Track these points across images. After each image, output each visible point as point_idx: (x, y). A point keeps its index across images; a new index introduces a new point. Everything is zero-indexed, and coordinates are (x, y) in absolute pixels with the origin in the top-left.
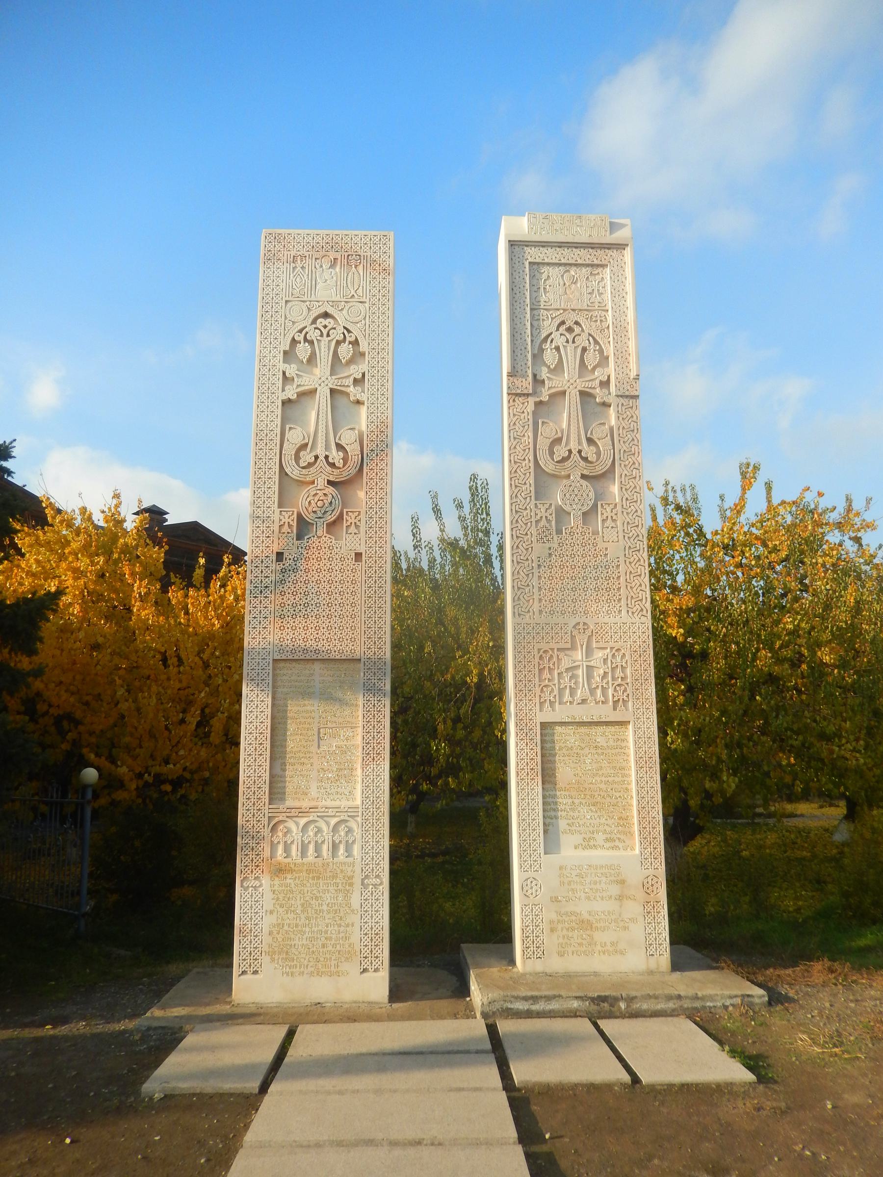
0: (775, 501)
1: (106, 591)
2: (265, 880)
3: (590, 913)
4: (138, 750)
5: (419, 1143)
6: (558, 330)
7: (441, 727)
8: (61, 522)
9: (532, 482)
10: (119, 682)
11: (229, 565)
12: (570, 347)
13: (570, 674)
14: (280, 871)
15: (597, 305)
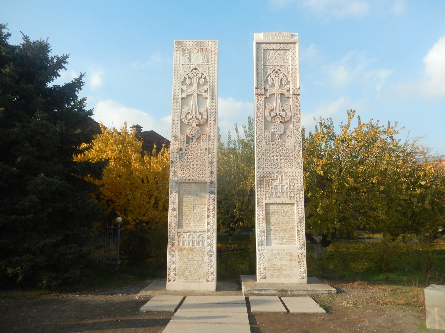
0: (362, 124)
2: (177, 252)
3: (281, 265)
7: (237, 205)
8: (107, 133)
9: (263, 124)
10: (128, 189)
11: (165, 147)
12: (277, 78)
14: (181, 249)
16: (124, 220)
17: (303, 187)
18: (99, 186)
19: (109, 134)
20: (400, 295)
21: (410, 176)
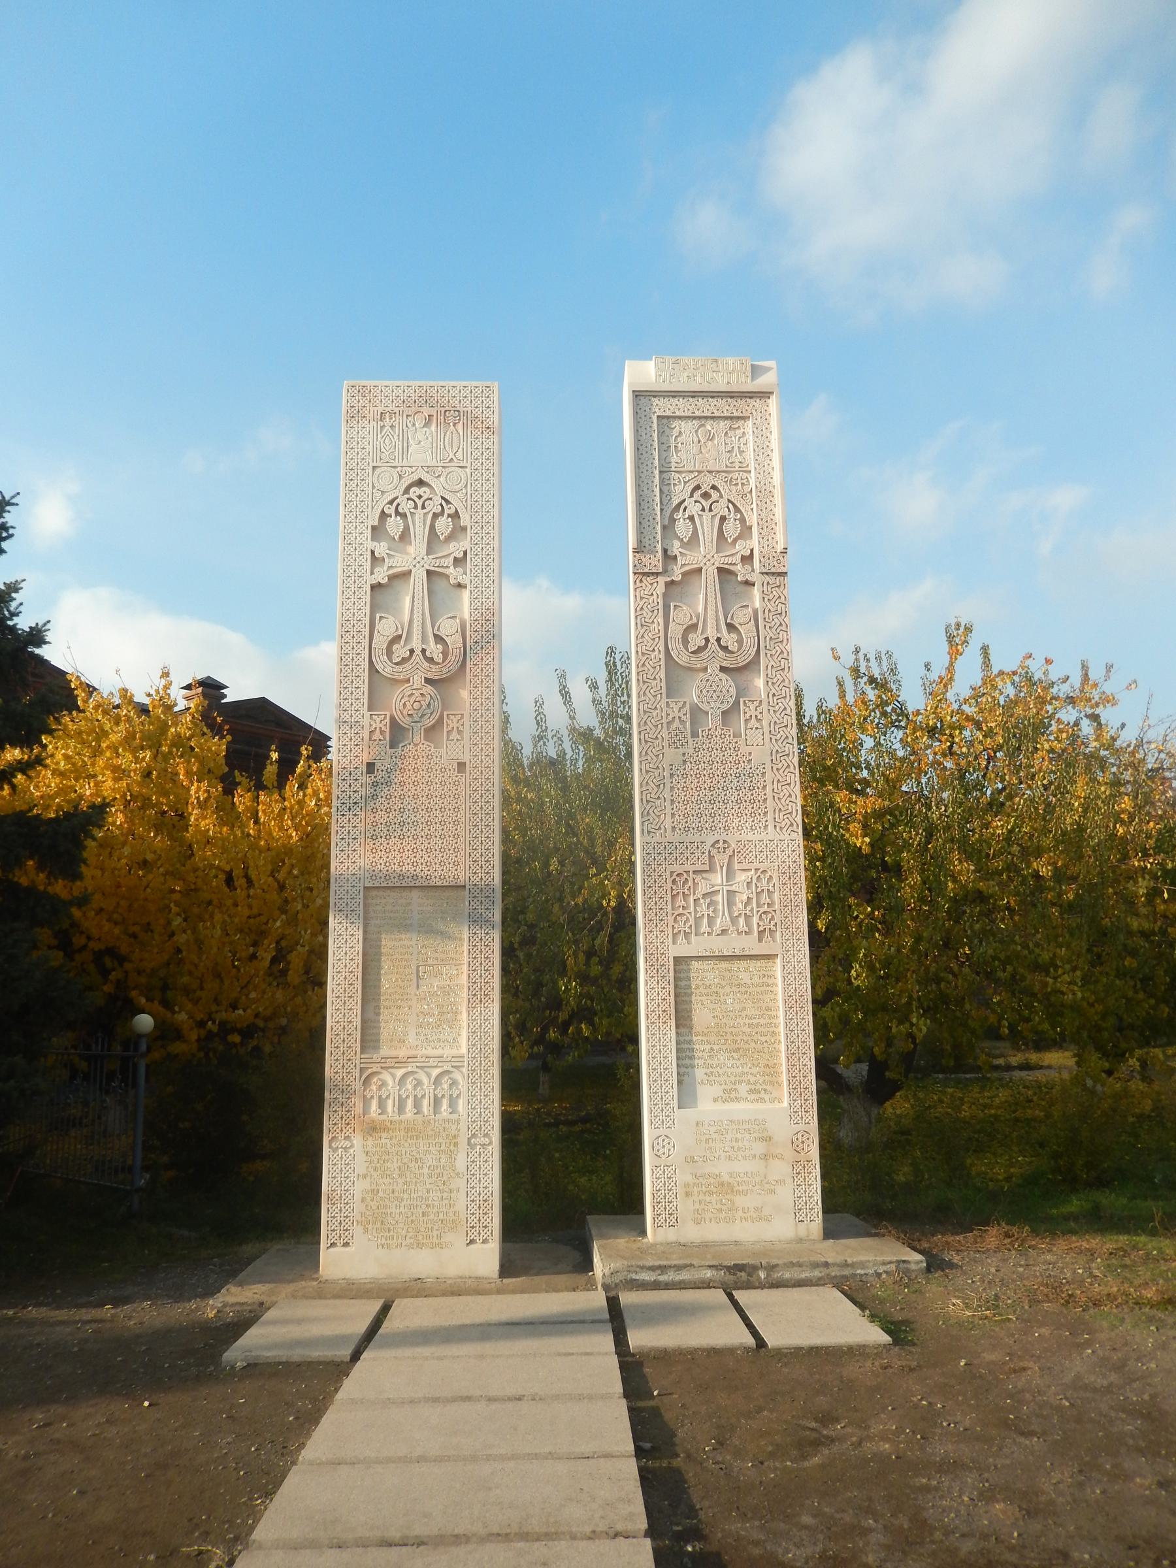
0: (995, 671)
1: (155, 793)
2: (357, 1140)
4: (199, 993)
5: (520, 1399)
6: (692, 496)
8: (96, 708)
9: (663, 676)
10: (174, 909)
11: (308, 757)
12: (707, 516)
13: (708, 901)
14: (373, 1129)
15: (737, 465)
16: (160, 1024)
17: (802, 897)
18: (71, 903)
19: (105, 712)
20: (1141, 1270)
21: (1158, 849)
